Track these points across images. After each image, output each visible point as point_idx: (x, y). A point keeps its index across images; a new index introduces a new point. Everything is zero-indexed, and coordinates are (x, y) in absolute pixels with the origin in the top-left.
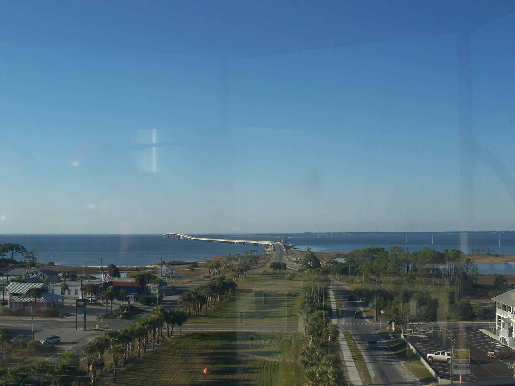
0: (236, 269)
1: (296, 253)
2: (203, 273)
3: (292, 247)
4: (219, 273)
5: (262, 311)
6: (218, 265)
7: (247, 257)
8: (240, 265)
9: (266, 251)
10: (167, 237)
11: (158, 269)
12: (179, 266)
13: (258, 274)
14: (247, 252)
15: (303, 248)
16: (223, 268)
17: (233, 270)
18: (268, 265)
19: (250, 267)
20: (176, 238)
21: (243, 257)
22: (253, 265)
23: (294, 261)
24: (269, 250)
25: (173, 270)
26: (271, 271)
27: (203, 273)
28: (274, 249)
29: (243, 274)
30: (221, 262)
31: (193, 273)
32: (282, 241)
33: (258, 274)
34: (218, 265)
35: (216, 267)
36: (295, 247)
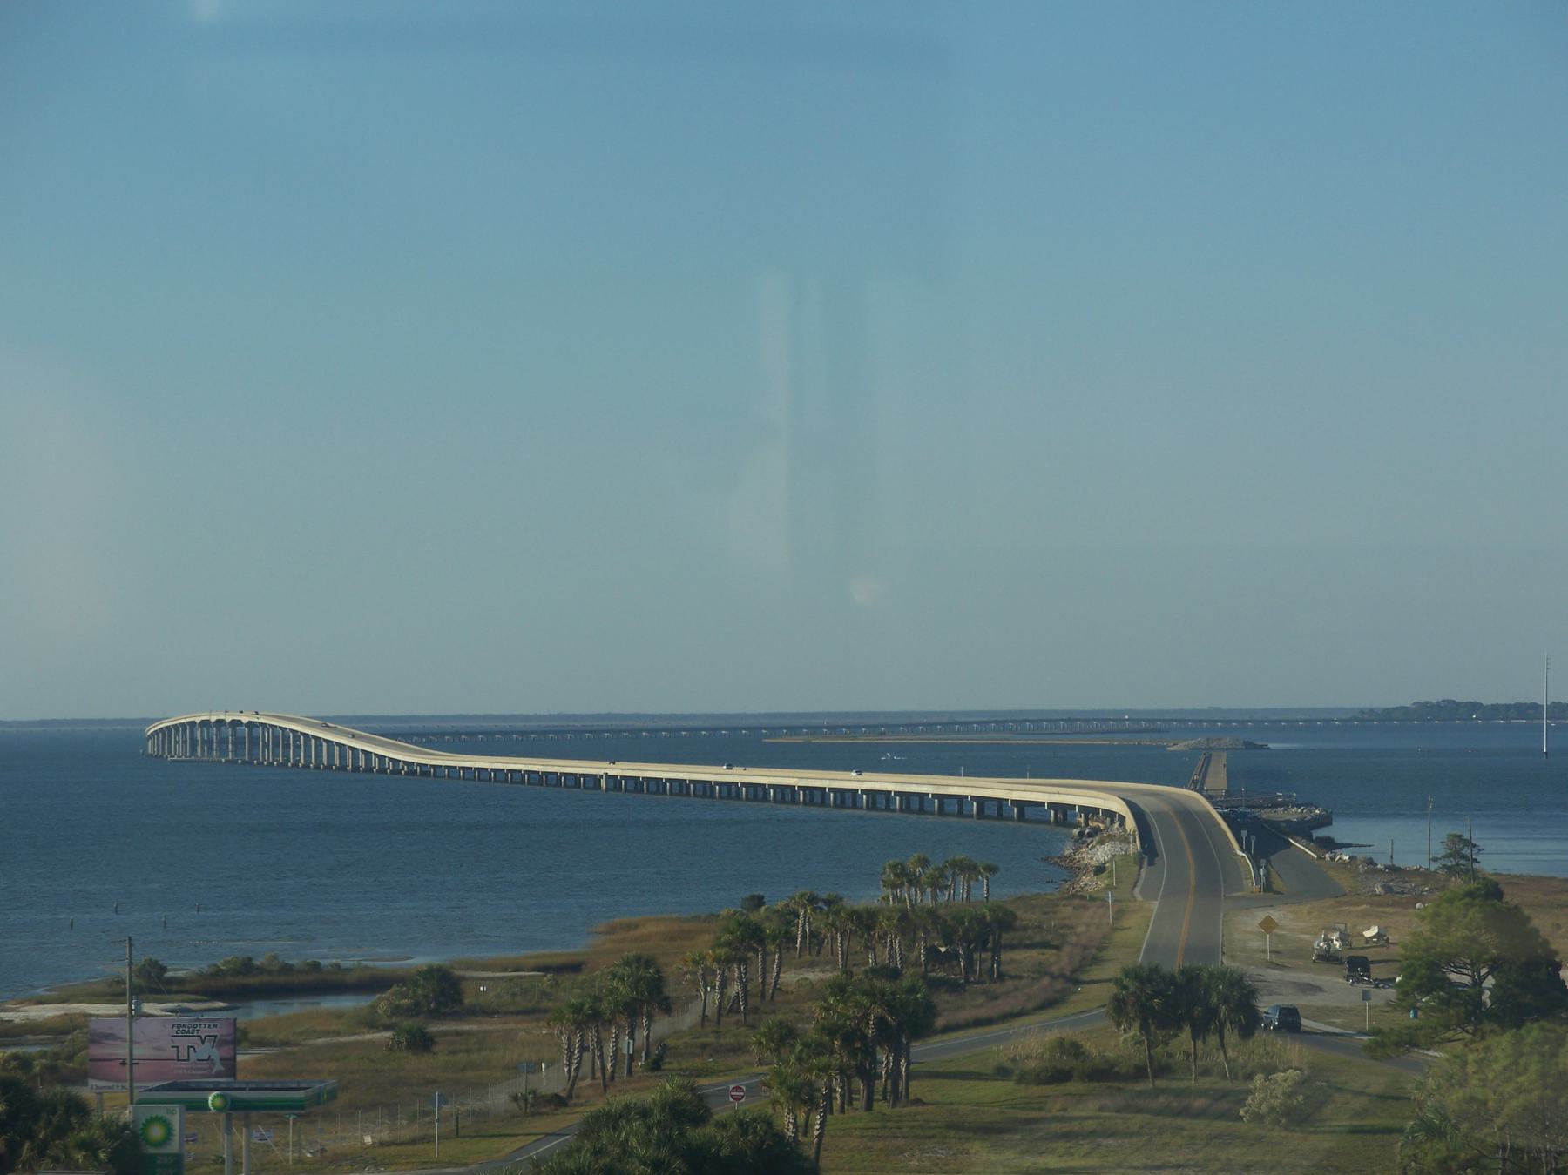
0: (810, 1030)
1: (1345, 881)
2: (513, 1069)
3: (1303, 829)
4: (656, 1065)
5: (342, 1039)
6: (650, 993)
7: (907, 923)
8: (839, 989)
9: (1074, 870)
10: (177, 751)
11: (98, 1038)
12: (295, 1008)
13: (1002, 1073)
14: (903, 876)
15: (1411, 843)
16: (687, 1020)
17: (784, 1036)
18: (1096, 995)
19: (930, 1010)
20: (265, 755)
21: (866, 921)
22: (955, 988)
23: (1328, 957)
24: (1101, 853)
25: (238, 1038)
26: (1119, 1042)
27: (513, 1069)
28: (1149, 850)
29: (869, 1077)
30: (675, 967)
31: (416, 1064)
32: (1218, 780)
33: (1002, 1073)
34: (650, 993)
35: (633, 1011)
36: (1338, 830)
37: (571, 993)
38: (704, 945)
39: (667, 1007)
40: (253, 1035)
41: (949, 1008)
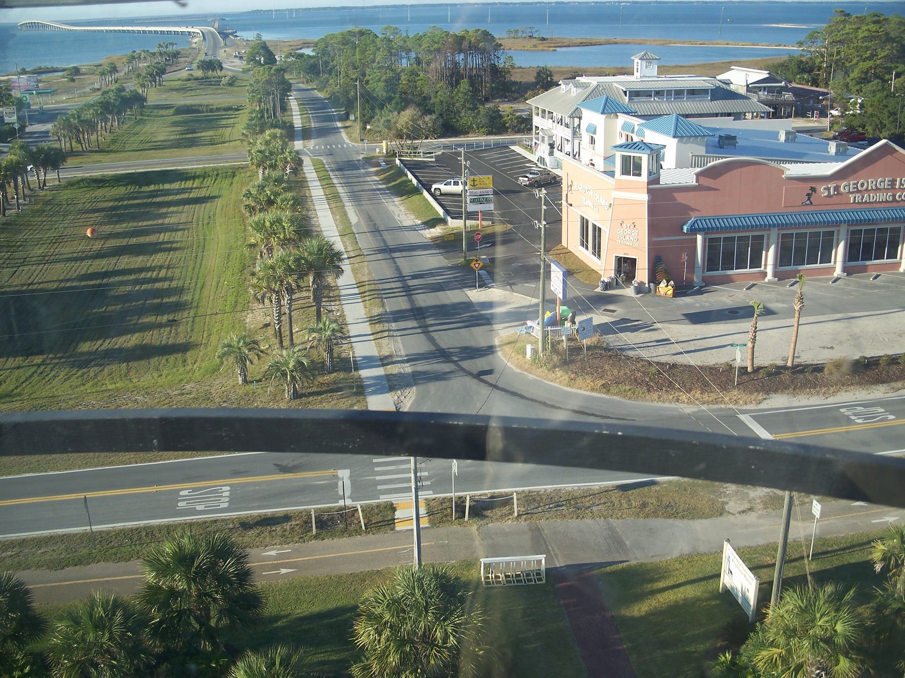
2: (89, 84)
8: (149, 66)
16: (122, 74)
17: (139, 75)
26: (199, 73)
27: (89, 84)
29: (155, 82)
30: (119, 66)
31: (72, 84)
34: (114, 69)
35: (111, 72)
37: (100, 69)
38: (124, 60)
39: (117, 71)
40: (740, 142)
41: (168, 69)
